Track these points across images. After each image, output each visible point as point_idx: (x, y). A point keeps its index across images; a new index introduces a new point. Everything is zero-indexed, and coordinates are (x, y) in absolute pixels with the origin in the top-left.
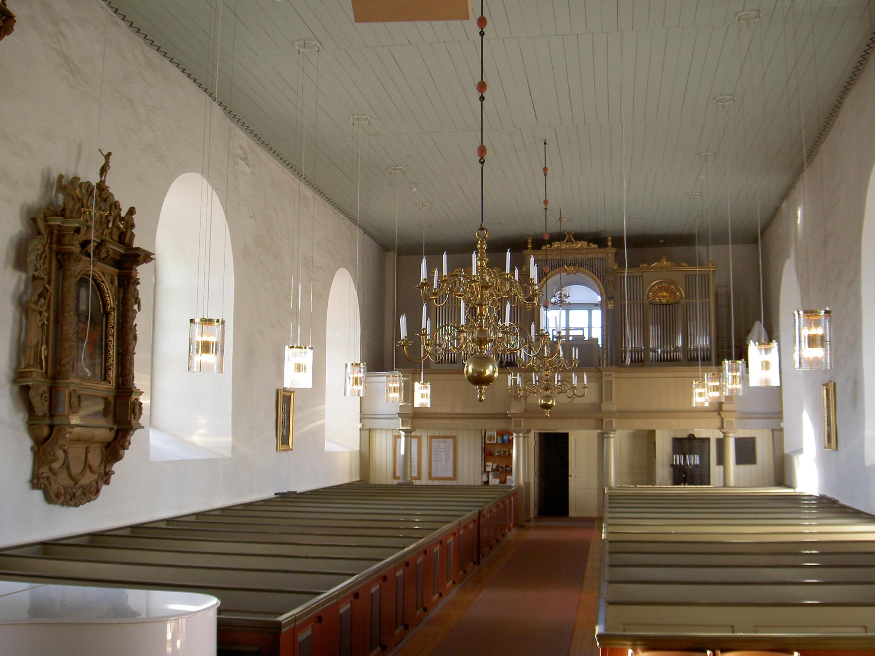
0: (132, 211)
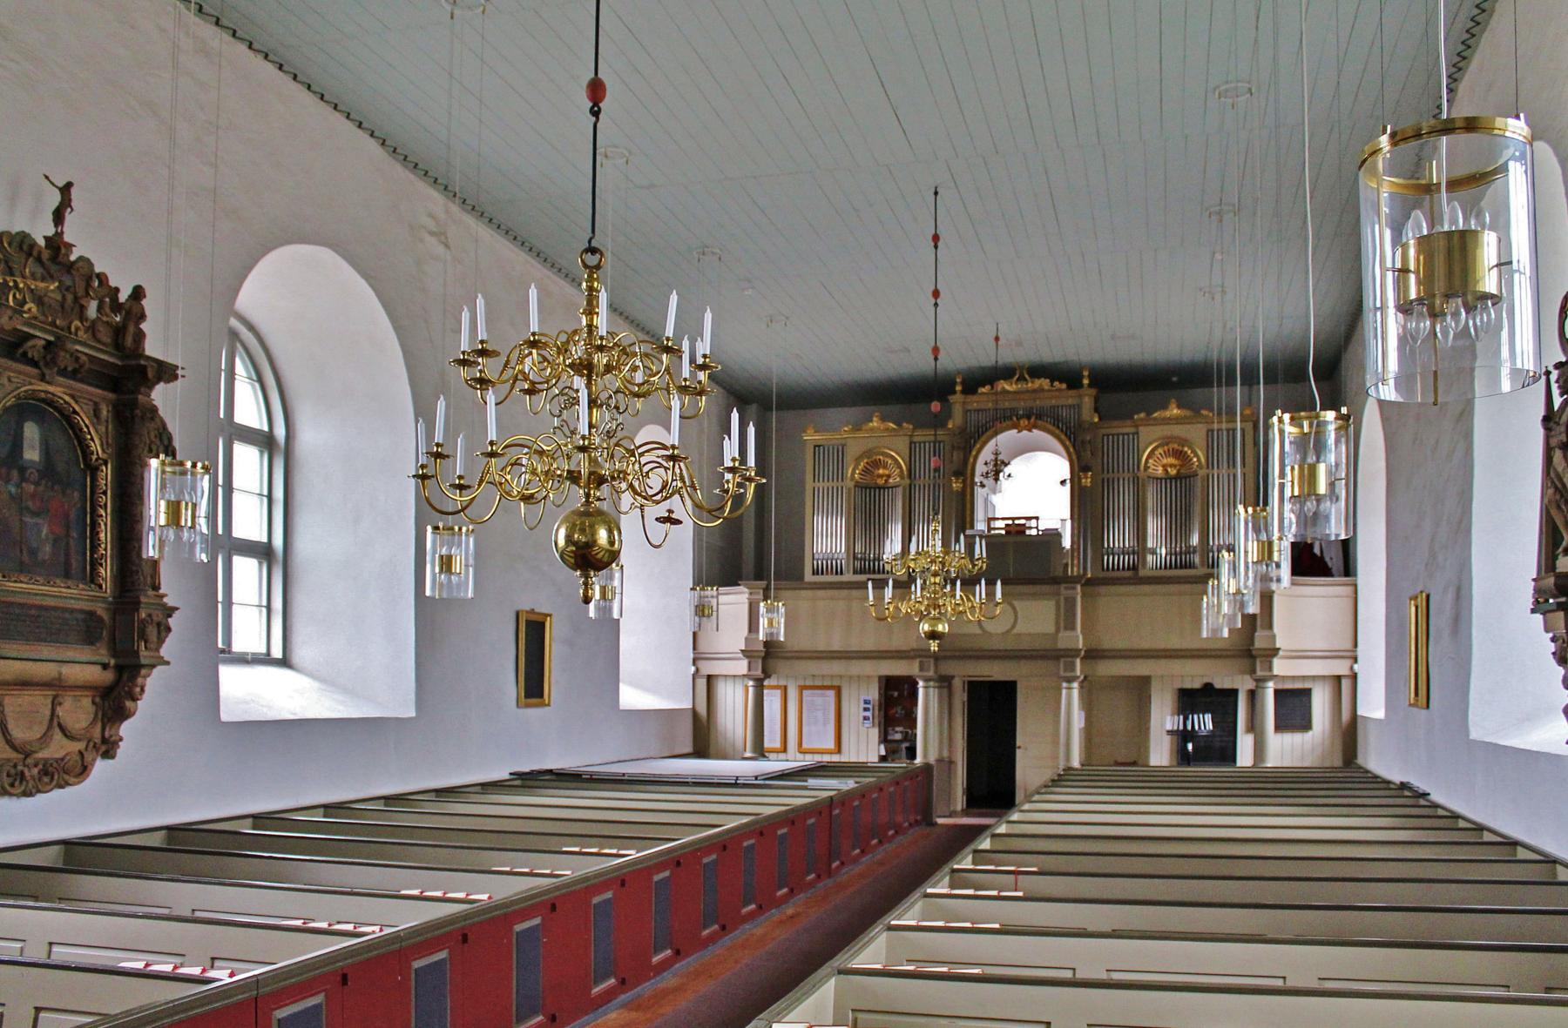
0: (138, 293)
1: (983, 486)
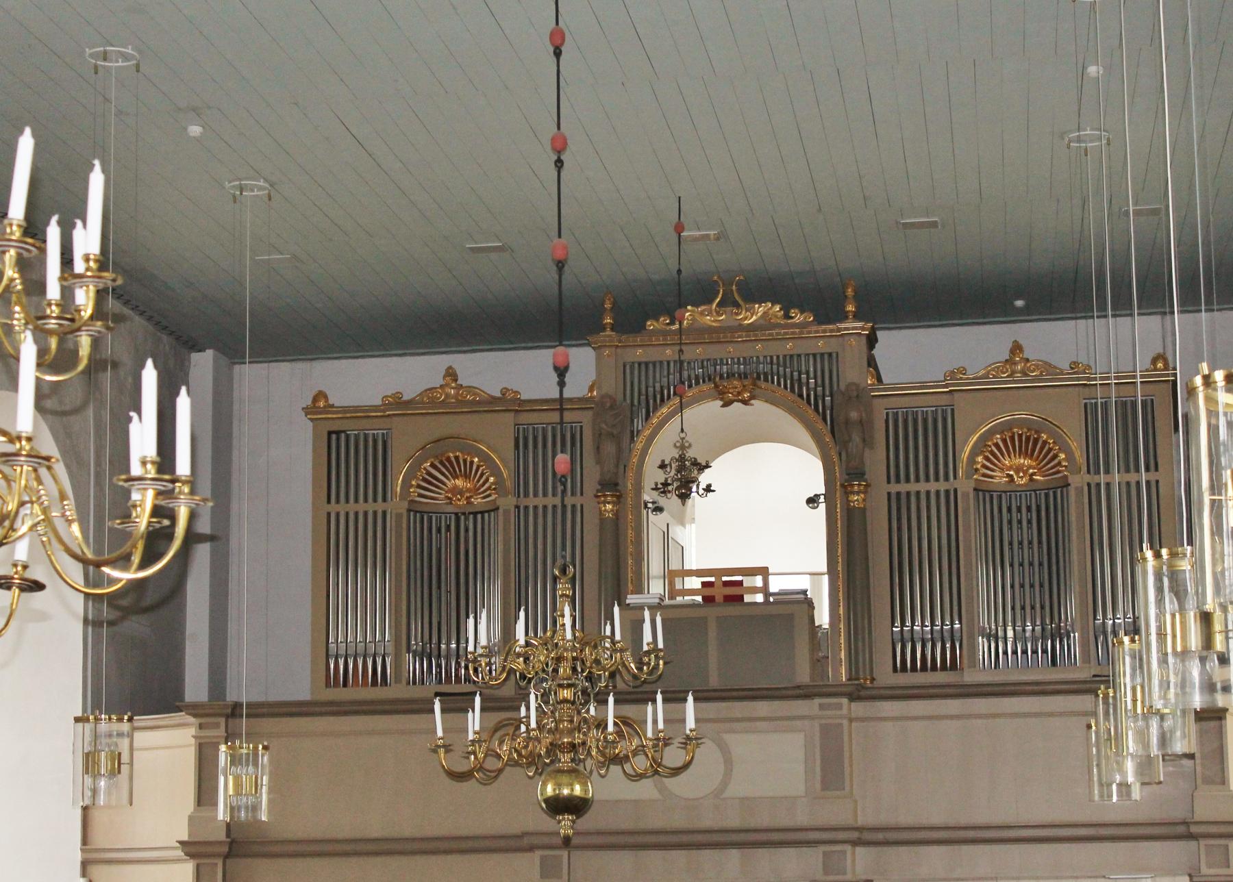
1: (658, 509)
